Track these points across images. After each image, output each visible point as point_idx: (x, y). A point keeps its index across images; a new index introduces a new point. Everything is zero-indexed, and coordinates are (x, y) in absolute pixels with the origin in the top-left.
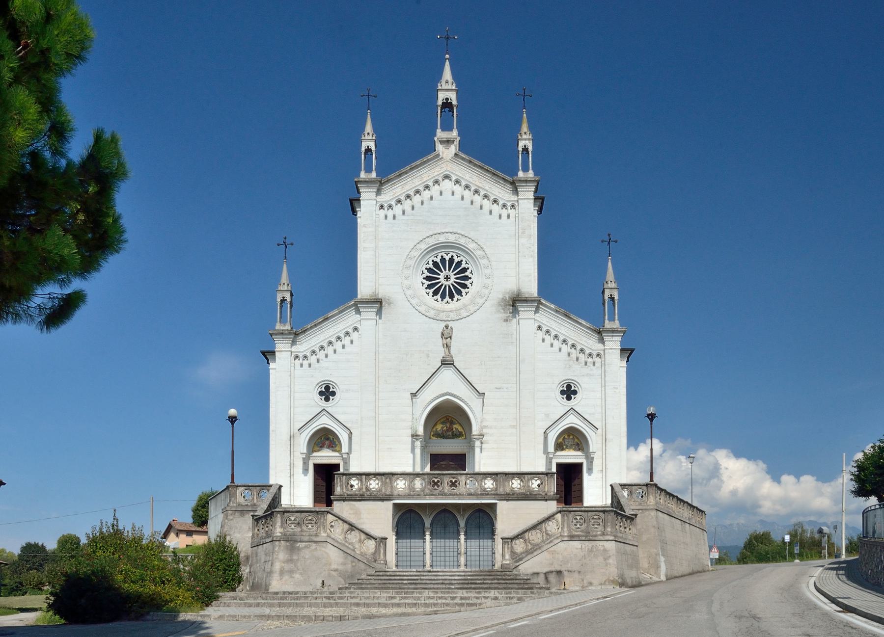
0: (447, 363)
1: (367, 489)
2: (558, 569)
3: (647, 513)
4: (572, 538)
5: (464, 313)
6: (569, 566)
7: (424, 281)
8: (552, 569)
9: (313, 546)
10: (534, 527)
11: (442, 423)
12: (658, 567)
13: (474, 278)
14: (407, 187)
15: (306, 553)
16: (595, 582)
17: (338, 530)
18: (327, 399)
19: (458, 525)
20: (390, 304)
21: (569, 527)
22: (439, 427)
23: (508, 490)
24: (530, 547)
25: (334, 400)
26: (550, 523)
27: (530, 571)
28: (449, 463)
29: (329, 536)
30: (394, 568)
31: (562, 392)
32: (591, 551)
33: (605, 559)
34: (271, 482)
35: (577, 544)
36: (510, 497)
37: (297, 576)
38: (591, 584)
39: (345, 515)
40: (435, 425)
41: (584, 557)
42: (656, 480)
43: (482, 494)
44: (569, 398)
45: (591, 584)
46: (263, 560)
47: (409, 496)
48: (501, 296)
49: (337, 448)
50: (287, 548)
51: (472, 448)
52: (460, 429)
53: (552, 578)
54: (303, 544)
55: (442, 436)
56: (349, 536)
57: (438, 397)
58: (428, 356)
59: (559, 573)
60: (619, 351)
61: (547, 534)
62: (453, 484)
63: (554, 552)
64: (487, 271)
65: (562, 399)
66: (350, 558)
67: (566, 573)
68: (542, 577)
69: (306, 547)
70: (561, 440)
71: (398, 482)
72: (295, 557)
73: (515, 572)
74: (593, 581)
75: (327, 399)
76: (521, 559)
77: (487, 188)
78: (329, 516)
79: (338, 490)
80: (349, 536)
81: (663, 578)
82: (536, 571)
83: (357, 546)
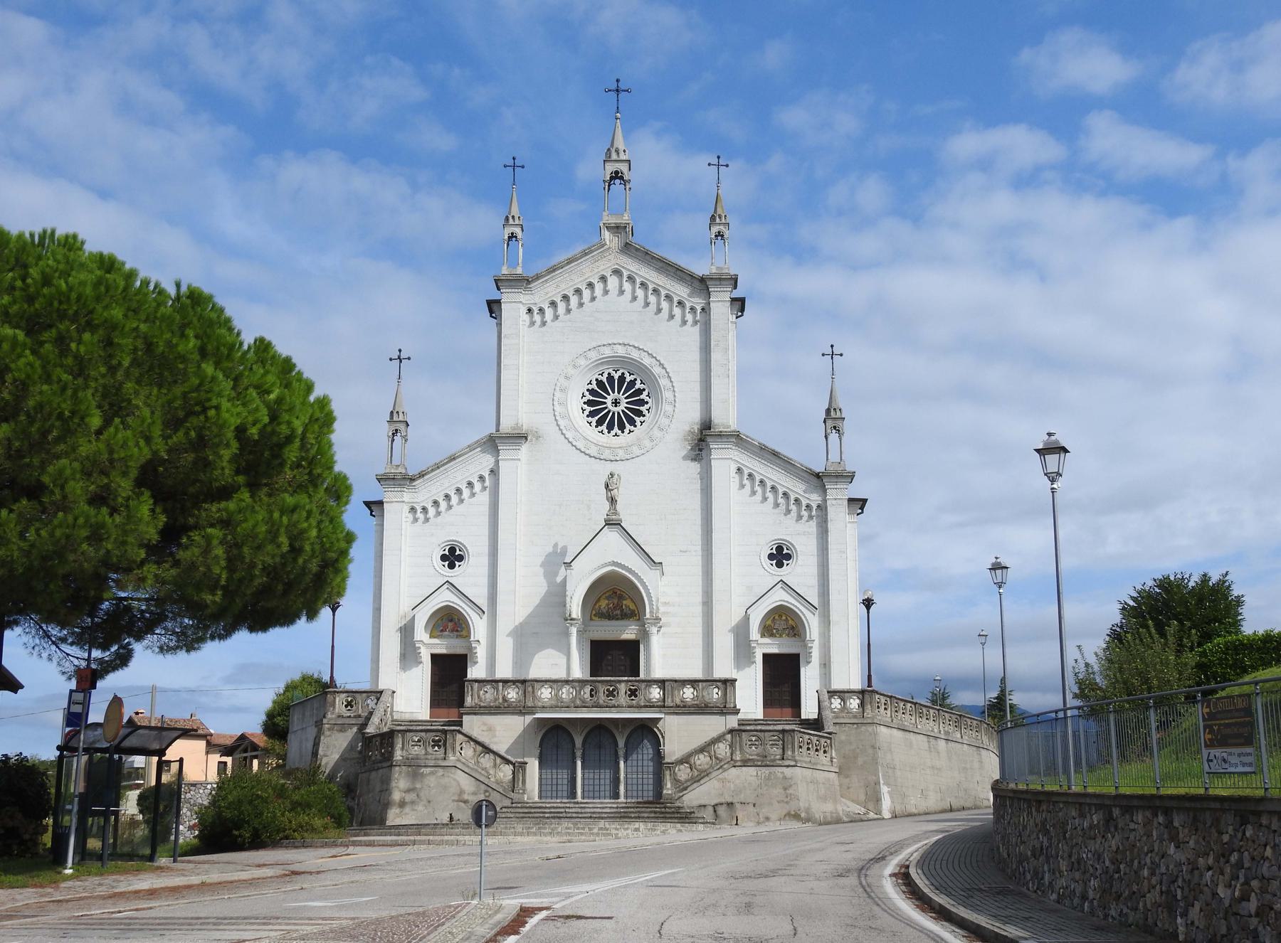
0: (612, 522)
1: (505, 699)
2: (730, 800)
3: (863, 728)
4: (745, 763)
5: (636, 451)
6: (742, 798)
7: (585, 406)
8: (723, 801)
9: (441, 772)
10: (702, 750)
11: (608, 598)
12: (878, 800)
13: (639, 430)
14: (563, 286)
15: (431, 781)
16: (774, 816)
17: (469, 751)
18: (452, 566)
19: (617, 745)
20: (538, 438)
21: (741, 749)
22: (603, 603)
23: (678, 701)
24: (696, 773)
25: (460, 568)
26: (721, 745)
27: (696, 803)
28: (615, 659)
29: (459, 760)
30: (536, 799)
31: (771, 557)
32: (768, 778)
33: (785, 789)
34: (381, 687)
35: (752, 771)
36: (684, 709)
37: (420, 808)
38: (767, 819)
39: (475, 734)
40: (599, 600)
41: (760, 786)
42: (875, 686)
43: (646, 706)
44: (780, 565)
45: (767, 819)
46: (378, 789)
47: (553, 708)
48: (687, 428)
49: (464, 633)
50: (408, 774)
51: (645, 634)
52: (632, 607)
53: (722, 811)
54: (429, 770)
55: (609, 616)
56: (482, 760)
57: (600, 568)
58: (589, 507)
59: (730, 805)
60: (846, 503)
61: (717, 758)
62: (611, 694)
63: (723, 781)
64: (656, 433)
65: (770, 566)
66: (483, 787)
67: (738, 806)
68: (711, 809)
69: (432, 773)
70: (769, 622)
71: (543, 690)
72: (418, 786)
73: (678, 804)
74: (770, 815)
75: (452, 566)
76: (685, 789)
77: (668, 286)
78: (460, 737)
79: (469, 701)
80: (482, 760)
81: (887, 815)
82: (703, 802)
83: (492, 772)
